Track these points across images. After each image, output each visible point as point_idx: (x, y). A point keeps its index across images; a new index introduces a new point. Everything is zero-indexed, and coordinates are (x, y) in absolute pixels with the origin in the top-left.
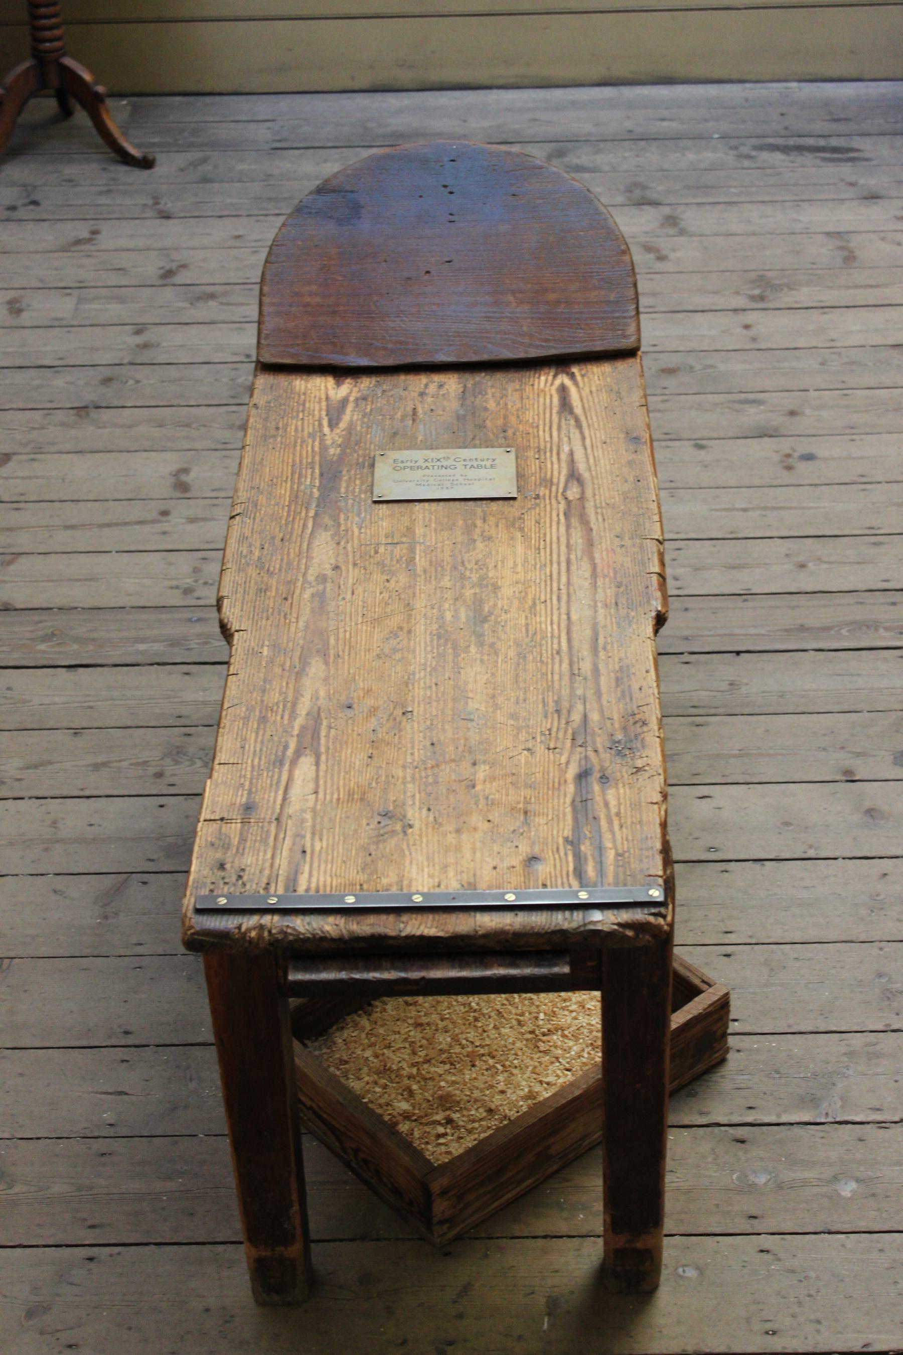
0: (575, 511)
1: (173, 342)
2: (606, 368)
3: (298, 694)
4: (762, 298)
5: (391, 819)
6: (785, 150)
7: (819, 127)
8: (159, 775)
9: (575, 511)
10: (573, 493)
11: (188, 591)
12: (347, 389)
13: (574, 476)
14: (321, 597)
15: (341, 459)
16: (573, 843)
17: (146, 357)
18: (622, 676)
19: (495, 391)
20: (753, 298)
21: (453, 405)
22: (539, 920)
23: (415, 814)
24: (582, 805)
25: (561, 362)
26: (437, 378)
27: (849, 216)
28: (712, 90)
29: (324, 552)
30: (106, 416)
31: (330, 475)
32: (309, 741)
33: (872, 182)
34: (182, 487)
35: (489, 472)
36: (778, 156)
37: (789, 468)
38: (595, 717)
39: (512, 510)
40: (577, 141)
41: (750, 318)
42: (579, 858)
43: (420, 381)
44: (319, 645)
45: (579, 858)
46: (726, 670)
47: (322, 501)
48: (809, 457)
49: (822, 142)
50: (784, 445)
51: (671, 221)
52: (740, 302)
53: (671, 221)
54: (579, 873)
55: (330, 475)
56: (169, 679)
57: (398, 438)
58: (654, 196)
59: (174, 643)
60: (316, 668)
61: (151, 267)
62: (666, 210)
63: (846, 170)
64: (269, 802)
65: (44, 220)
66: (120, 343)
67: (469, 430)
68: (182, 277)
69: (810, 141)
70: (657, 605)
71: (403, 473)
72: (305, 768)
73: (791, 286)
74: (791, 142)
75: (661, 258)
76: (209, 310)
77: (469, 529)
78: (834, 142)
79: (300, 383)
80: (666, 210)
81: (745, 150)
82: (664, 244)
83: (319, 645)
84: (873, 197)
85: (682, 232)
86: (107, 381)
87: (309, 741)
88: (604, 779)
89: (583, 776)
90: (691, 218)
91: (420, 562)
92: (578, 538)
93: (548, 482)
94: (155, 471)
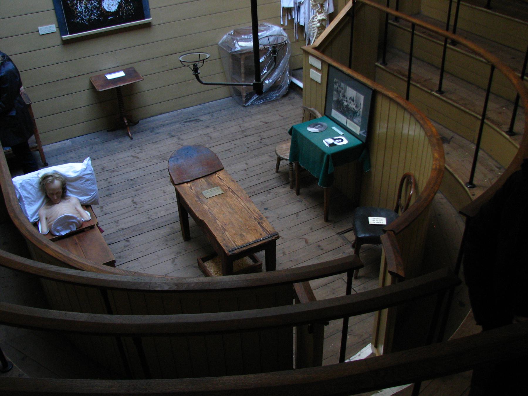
0: (232, 192)
1: (115, 180)
11: (149, 218)
12: (189, 185)
13: (229, 188)
14: (211, 214)
16: (264, 231)
17: (111, 184)
18: (254, 211)
23: (243, 234)
24: (261, 226)
25: (215, 172)
26: (200, 179)
28: (168, 114)
29: (206, 207)
31: (198, 197)
34: (135, 203)
36: (188, 123)
40: (154, 128)
43: (198, 180)
55: (198, 197)
60: (218, 221)
63: (200, 122)
67: (212, 185)
76: (116, 173)
78: (196, 118)
82: (180, 143)
83: (215, 219)
84: (207, 127)
85: (182, 140)
89: (259, 223)
90: (182, 137)
93: (226, 190)
94: (129, 201)
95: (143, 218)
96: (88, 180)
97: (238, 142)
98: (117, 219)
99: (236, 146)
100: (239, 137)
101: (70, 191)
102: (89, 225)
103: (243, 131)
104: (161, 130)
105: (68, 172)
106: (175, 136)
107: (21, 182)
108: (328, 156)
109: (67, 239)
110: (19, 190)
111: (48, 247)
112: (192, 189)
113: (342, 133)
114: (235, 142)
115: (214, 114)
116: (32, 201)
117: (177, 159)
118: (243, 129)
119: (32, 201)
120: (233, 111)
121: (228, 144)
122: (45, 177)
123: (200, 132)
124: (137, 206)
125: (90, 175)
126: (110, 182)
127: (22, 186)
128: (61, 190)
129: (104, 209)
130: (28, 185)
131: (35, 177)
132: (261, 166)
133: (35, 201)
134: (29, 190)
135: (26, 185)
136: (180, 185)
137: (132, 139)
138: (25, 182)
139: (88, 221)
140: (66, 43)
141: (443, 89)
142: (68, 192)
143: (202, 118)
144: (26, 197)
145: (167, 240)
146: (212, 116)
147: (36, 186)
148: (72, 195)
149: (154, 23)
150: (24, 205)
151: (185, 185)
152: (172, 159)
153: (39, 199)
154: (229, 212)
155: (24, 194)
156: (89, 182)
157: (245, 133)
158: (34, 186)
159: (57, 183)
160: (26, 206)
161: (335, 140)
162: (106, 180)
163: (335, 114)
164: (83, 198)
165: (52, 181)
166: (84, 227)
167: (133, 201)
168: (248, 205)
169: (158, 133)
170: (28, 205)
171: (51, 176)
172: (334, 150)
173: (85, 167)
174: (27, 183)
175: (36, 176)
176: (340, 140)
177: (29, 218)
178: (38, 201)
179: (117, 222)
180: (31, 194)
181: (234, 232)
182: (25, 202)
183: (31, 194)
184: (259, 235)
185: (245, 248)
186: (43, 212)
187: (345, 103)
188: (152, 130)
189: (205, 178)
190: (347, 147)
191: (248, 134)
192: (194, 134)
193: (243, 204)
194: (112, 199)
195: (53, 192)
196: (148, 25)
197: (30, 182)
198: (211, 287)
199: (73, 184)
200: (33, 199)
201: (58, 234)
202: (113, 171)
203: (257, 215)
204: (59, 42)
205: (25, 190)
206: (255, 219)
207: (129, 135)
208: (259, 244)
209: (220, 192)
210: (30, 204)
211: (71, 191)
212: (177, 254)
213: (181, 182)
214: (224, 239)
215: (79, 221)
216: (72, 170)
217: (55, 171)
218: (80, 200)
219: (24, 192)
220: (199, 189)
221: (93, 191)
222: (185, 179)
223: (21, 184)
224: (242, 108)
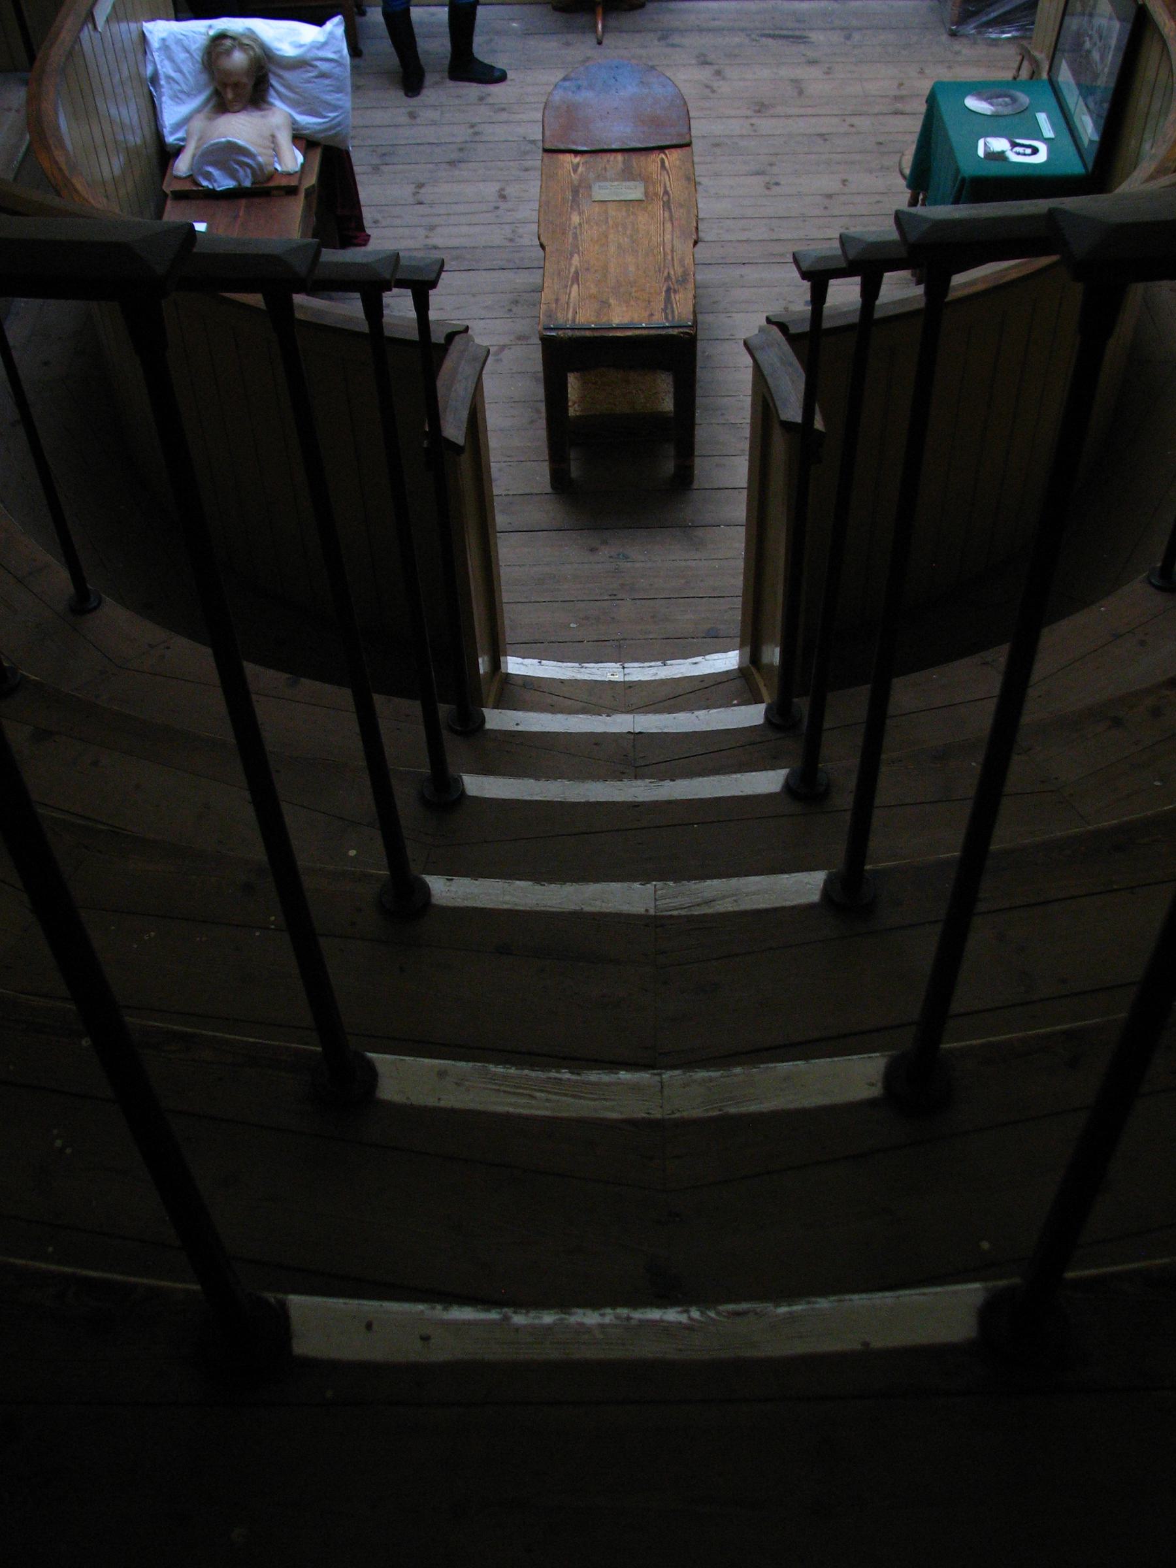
2: (679, 151)
3: (570, 265)
4: (759, 111)
5: (605, 304)
6: (773, 37)
7: (790, 24)
8: (510, 310)
9: (667, 205)
10: (665, 198)
11: (511, 240)
12: (577, 160)
13: (666, 192)
14: (575, 237)
15: (579, 185)
16: (665, 310)
18: (681, 260)
19: (636, 160)
20: (755, 111)
21: (620, 165)
22: (653, 332)
25: (661, 149)
26: (614, 155)
27: (802, 73)
29: (576, 219)
30: (462, 165)
31: (575, 192)
32: (576, 279)
33: (811, 54)
34: (503, 197)
35: (634, 191)
36: (770, 41)
37: (768, 188)
38: (672, 273)
39: (644, 205)
41: (753, 121)
42: (666, 314)
43: (606, 157)
44: (575, 250)
45: (666, 314)
46: (738, 271)
47: (574, 201)
48: (777, 184)
49: (791, 33)
50: (767, 178)
51: (718, 73)
52: (749, 113)
53: (718, 73)
54: (666, 318)
55: (575, 192)
56: (509, 275)
57: (600, 178)
58: (709, 60)
59: (509, 261)
62: (716, 67)
63: (802, 47)
64: (564, 299)
65: (697, 228)
66: (462, 134)
67: (628, 175)
68: (490, 100)
69: (785, 32)
70: (694, 237)
71: (602, 191)
72: (575, 287)
73: (773, 106)
74: (777, 32)
75: (713, 92)
76: (504, 116)
77: (628, 211)
78: (797, 33)
79: (561, 157)
80: (716, 67)
81: (753, 36)
82: (715, 85)
83: (575, 250)
84: (812, 62)
85: (724, 79)
86: (461, 150)
87: (576, 279)
88: (675, 292)
89: (668, 290)
91: (610, 222)
92: (667, 214)
93: (656, 194)
94: (491, 189)
95: (497, 236)
96: (323, 75)
97: (863, 123)
98: (435, 221)
99: (853, 130)
100: (876, 109)
101: (276, 91)
102: (284, 182)
103: (897, 98)
104: (686, 41)
105: (280, 40)
106: (711, 64)
107: (164, 35)
108: (963, 180)
109: (223, 204)
110: (156, 54)
112: (575, 171)
113: (1048, 133)
114: (856, 120)
115: (856, 36)
116: (182, 92)
117: (579, 88)
118: (904, 92)
119: (182, 92)
120: (915, 39)
121: (835, 120)
122: (222, 36)
123: (785, 72)
124: (504, 206)
125: (333, 65)
126: (476, 134)
127: (165, 47)
128: (248, 82)
129: (423, 191)
130: (180, 49)
131: (201, 33)
132: (878, 198)
133: (188, 95)
134: (179, 61)
135: (173, 47)
136: (555, 156)
137: (600, 43)
138: (176, 37)
139: (289, 174)
142: (272, 92)
143: (814, 36)
144: (168, 78)
146: (848, 37)
147: (198, 56)
148: (278, 103)
150: (161, 95)
151: (569, 158)
152: (567, 84)
153: (200, 92)
154: (619, 246)
155: (165, 68)
156: (327, 82)
157: (899, 106)
158: (191, 55)
159: (239, 58)
160: (164, 99)
161: (1014, 145)
162: (472, 126)
163: (1065, 75)
164: (304, 120)
165: (229, 52)
166: (272, 184)
167: (503, 189)
168: (677, 243)
169: (673, 46)
170: (172, 98)
171: (233, 38)
172: (995, 170)
173: (322, 39)
174: (179, 42)
175: (203, 30)
176: (1029, 151)
177: (166, 132)
178: (195, 96)
179: (432, 228)
180: (180, 71)
181: (594, 290)
182: (166, 88)
183: (180, 71)
184: (646, 314)
185: (588, 334)
186: (198, 124)
187: (1088, 45)
188: (665, 35)
189: (626, 155)
190: (1038, 172)
191: (908, 108)
192: (766, 73)
193: (668, 237)
194: (457, 173)
195: (243, 83)
197: (186, 42)
198: (328, 321)
199: (288, 75)
200: (185, 88)
201: (205, 183)
202: (503, 109)
203: (680, 271)
205: (171, 60)
206: (668, 277)
207: (596, 31)
208: (629, 333)
210: (177, 98)
211: (280, 96)
212: (519, 338)
213: (562, 147)
214: (557, 300)
215: (260, 165)
216: (293, 39)
217: (249, 29)
218: (294, 122)
219: (166, 63)
220: (592, 176)
221: (335, 108)
222: (574, 143)
223: (164, 40)
224: (944, 38)
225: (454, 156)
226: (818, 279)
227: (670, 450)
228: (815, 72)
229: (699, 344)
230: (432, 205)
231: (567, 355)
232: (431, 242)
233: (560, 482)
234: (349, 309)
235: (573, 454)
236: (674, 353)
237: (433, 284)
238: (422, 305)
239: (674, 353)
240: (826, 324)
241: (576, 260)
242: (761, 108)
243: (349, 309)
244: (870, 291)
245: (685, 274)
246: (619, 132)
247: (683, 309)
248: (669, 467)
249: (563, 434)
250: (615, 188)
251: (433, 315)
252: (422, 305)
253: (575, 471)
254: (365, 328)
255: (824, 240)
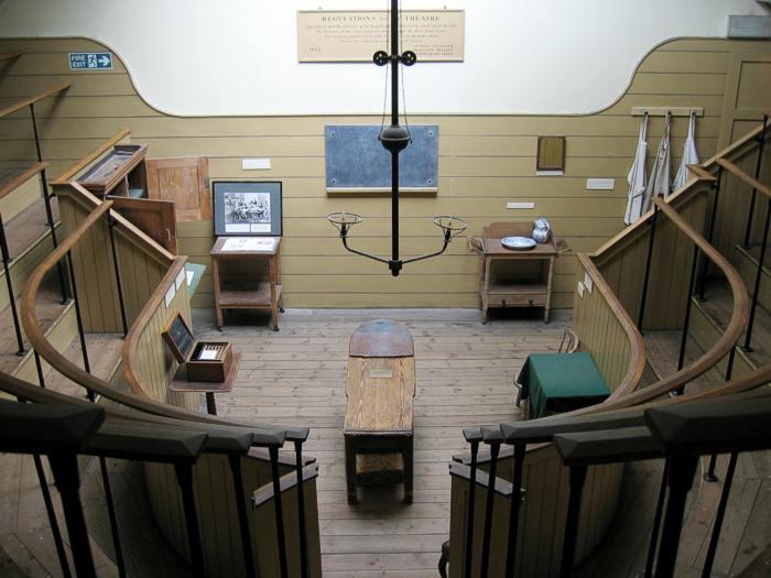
5: (374, 420)
27: (469, 340)
29: (362, 384)
31: (363, 373)
40: (413, 321)
61: (34, 560)
66: (315, 365)
97: (499, 362)
111: (131, 371)
123: (464, 340)
140: (331, 196)
141: (751, 345)
145: (428, 470)
149: (439, 195)
196: (432, 195)
204: (324, 194)
209: (390, 376)
225: (313, 375)
226: (474, 443)
227: (402, 486)
228: (477, 339)
229: (415, 440)
230: (300, 397)
231: (358, 445)
232: (300, 414)
233: (352, 500)
234: (264, 452)
235: (358, 489)
236: (401, 445)
237: (305, 440)
238: (298, 449)
239: (401, 445)
240: (478, 460)
241: (361, 402)
242: (452, 356)
243: (264, 452)
244: (495, 450)
245: (409, 409)
246: (384, 350)
247: (407, 424)
248: (402, 494)
249: (353, 479)
250: (378, 371)
251: (303, 454)
252: (298, 449)
253: (359, 497)
254: (269, 458)
255: (474, 430)
